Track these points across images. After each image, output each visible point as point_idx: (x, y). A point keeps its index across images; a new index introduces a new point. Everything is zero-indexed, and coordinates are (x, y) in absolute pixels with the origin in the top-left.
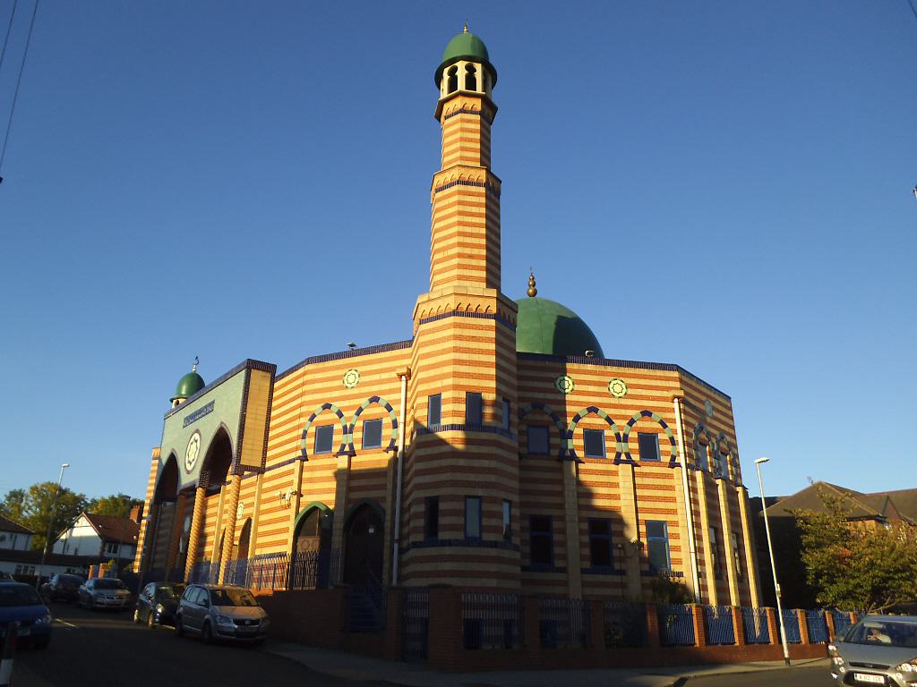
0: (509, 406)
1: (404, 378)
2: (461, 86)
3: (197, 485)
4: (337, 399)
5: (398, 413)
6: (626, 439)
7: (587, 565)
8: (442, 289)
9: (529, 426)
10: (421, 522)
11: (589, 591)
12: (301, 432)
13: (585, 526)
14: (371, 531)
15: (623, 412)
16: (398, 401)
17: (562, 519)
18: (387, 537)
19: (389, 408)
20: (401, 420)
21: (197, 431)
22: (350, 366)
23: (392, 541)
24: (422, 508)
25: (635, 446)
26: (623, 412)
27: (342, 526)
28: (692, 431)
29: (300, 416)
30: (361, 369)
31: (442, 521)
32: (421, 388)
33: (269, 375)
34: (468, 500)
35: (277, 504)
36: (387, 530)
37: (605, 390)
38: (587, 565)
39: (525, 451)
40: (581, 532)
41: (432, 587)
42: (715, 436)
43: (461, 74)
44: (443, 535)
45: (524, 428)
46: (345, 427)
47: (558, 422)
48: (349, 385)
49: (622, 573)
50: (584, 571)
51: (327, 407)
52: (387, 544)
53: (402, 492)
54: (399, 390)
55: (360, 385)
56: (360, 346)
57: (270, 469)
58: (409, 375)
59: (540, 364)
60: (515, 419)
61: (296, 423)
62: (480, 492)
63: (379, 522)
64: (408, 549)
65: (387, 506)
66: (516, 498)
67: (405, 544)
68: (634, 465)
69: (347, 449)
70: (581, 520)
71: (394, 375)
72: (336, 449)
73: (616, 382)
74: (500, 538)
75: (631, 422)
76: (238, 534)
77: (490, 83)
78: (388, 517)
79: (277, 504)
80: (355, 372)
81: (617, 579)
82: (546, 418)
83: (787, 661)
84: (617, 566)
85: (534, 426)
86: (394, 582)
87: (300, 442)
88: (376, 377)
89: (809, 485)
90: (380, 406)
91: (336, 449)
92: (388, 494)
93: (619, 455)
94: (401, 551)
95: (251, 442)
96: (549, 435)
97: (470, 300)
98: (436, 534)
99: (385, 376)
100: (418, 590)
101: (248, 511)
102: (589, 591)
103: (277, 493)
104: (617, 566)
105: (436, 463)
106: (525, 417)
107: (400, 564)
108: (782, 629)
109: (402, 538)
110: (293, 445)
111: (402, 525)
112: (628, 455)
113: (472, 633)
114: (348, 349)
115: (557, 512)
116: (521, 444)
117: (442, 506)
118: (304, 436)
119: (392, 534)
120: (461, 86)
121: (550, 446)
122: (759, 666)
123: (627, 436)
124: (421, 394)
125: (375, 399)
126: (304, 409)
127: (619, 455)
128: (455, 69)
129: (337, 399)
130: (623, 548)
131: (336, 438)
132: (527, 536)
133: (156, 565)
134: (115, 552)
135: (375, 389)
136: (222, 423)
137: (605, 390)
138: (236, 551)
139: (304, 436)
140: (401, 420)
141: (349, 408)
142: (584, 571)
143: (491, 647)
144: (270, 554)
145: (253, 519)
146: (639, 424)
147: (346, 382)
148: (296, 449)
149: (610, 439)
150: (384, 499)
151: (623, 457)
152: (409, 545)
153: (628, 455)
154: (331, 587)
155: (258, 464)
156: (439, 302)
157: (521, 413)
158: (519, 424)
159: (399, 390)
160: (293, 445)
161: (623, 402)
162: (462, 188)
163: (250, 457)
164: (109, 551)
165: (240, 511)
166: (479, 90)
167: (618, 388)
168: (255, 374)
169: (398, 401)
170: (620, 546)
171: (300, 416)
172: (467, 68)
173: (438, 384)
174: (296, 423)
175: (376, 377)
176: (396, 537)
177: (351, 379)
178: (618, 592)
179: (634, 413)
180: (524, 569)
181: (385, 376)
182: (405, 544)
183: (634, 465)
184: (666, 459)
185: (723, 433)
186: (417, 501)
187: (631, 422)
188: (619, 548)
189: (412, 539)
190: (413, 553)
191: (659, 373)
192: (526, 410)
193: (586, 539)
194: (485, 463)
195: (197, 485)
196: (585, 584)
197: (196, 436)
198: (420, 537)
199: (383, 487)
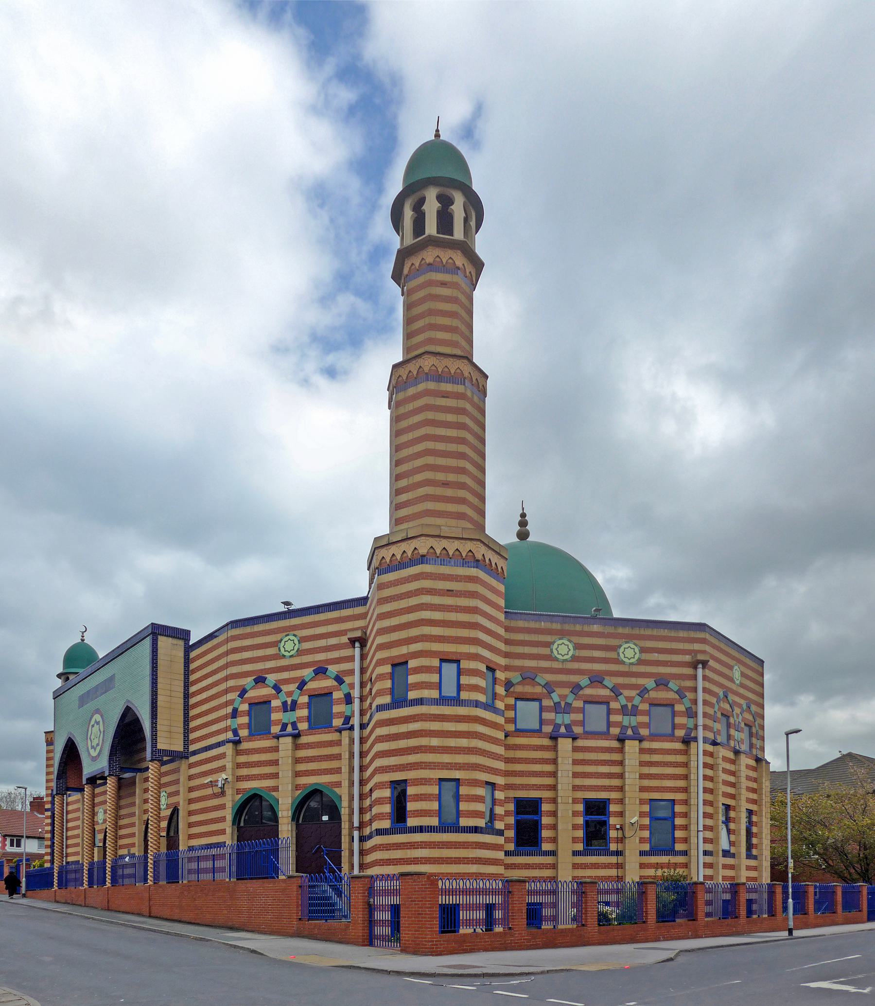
0: (493, 675)
1: (357, 644)
2: (431, 228)
3: (107, 774)
5: (352, 686)
6: (294, 706)
7: (580, 847)
8: (407, 529)
9: (517, 699)
10: (387, 808)
11: (580, 873)
12: (229, 709)
13: (580, 807)
14: (325, 818)
15: (633, 681)
16: (351, 672)
18: (345, 826)
19: (339, 680)
20: (356, 693)
21: (97, 711)
22: (286, 630)
23: (351, 828)
24: (387, 793)
26: (633, 681)
27: (290, 814)
28: (714, 700)
29: (227, 691)
30: (576, 640)
31: (411, 806)
32: (380, 655)
33: (181, 643)
34: (443, 783)
35: (209, 791)
36: (345, 817)
37: (545, 651)
38: (580, 847)
39: (511, 727)
40: (575, 814)
41: (403, 875)
42: (740, 706)
43: (431, 207)
44: (411, 822)
45: (511, 701)
46: (285, 703)
47: (621, 698)
48: (286, 654)
51: (260, 680)
52: (345, 832)
53: (361, 776)
54: (351, 659)
55: (300, 653)
56: (296, 606)
57: (195, 753)
58: (362, 641)
60: (500, 690)
61: (223, 699)
62: (457, 775)
63: (334, 811)
64: (370, 837)
65: (343, 792)
66: (500, 780)
67: (367, 831)
69: (289, 729)
70: (575, 801)
71: (344, 639)
73: (626, 645)
74: (481, 823)
75: (302, 684)
76: (164, 824)
77: (473, 223)
78: (345, 803)
79: (209, 791)
80: (292, 638)
81: (613, 859)
82: (538, 690)
83: (790, 932)
85: (522, 699)
86: (356, 872)
87: (229, 722)
88: (322, 643)
89: (839, 755)
90: (329, 677)
92: (344, 777)
94: (362, 839)
95: (167, 723)
96: (674, 714)
97: (445, 543)
98: (405, 821)
99: (333, 641)
100: (383, 877)
101: (174, 800)
102: (580, 873)
103: (207, 780)
104: (613, 847)
105: (402, 744)
106: (512, 689)
107: (362, 853)
108: (790, 900)
109: (362, 826)
110: (222, 725)
111: (362, 811)
113: (449, 918)
114: (282, 608)
115: (613, 795)
116: (508, 721)
117: (411, 791)
118: (235, 714)
119: (351, 822)
120: (431, 228)
121: (674, 727)
122: (762, 937)
123: (296, 701)
124: (381, 662)
126: (231, 683)
128: (422, 201)
130: (621, 828)
132: (511, 820)
133: (70, 859)
134: (18, 845)
136: (128, 701)
137: (545, 651)
138: (164, 842)
140: (356, 693)
141: (562, 684)
142: (575, 853)
143: (471, 931)
144: (207, 845)
145: (181, 808)
147: (282, 650)
148: (226, 730)
149: (277, 710)
150: (338, 784)
152: (371, 833)
153: (568, 727)
154: (281, 877)
155: (180, 748)
156: (404, 546)
157: (508, 685)
158: (506, 696)
159: (351, 659)
160: (222, 725)
161: (635, 669)
162: (432, 385)
163: (169, 739)
164: (12, 845)
165: (163, 801)
166: (458, 234)
168: (164, 642)
169: (351, 672)
170: (618, 827)
171: (227, 691)
172: (439, 198)
173: (404, 650)
174: (223, 699)
175: (322, 643)
176: (356, 824)
177: (289, 646)
178: (613, 872)
180: (507, 853)
181: (333, 641)
182: (367, 831)
184: (337, 722)
185: (750, 702)
186: (380, 786)
187: (302, 684)
188: (617, 829)
189: (376, 825)
190: (377, 840)
191: (682, 634)
192: (514, 681)
193: (580, 821)
194: (464, 742)
195: (107, 774)
196: (642, 866)
197: (97, 717)
198: (386, 824)
199: (338, 771)
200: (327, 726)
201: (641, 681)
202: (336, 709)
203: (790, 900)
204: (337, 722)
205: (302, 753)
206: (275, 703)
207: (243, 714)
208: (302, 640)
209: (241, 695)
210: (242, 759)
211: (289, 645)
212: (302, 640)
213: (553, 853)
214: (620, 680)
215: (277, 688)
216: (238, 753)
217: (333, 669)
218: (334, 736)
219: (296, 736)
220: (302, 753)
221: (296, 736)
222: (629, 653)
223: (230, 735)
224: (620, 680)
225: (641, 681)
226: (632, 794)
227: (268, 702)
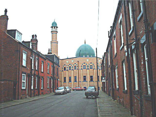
4: (93, 62)
7: (90, 81)
13: (90, 77)
17: (87, 76)
30: (89, 59)
49: (72, 82)
50: (63, 82)
55: (89, 61)
59: (75, 58)
68: (89, 69)
72: (66, 70)
81: (93, 82)
84: (93, 81)
91: (66, 70)
93: (87, 68)
98: (64, 79)
112: (88, 68)
125: (70, 64)
127: (87, 68)
129: (93, 62)
131: (66, 69)
135: (70, 63)
139: (62, 68)
142: (63, 82)
146: (83, 64)
151: (88, 69)
153: (88, 68)
167: (88, 60)
183: (89, 69)
184: (86, 69)
187: (89, 64)
200: (92, 69)
201: (89, 63)
202: (77, 67)
203: (149, 86)
204: (93, 68)
205: (74, 72)
206: (71, 67)
208: (68, 61)
210: (68, 72)
211: (72, 61)
212: (68, 61)
213: (87, 81)
214: (87, 63)
215: (71, 65)
216: (68, 72)
217: (92, 63)
218: (76, 70)
219: (73, 70)
220: (74, 72)
221: (73, 70)
223: (62, 70)
224: (87, 63)
225: (89, 63)
226: (88, 75)
227: (85, 66)
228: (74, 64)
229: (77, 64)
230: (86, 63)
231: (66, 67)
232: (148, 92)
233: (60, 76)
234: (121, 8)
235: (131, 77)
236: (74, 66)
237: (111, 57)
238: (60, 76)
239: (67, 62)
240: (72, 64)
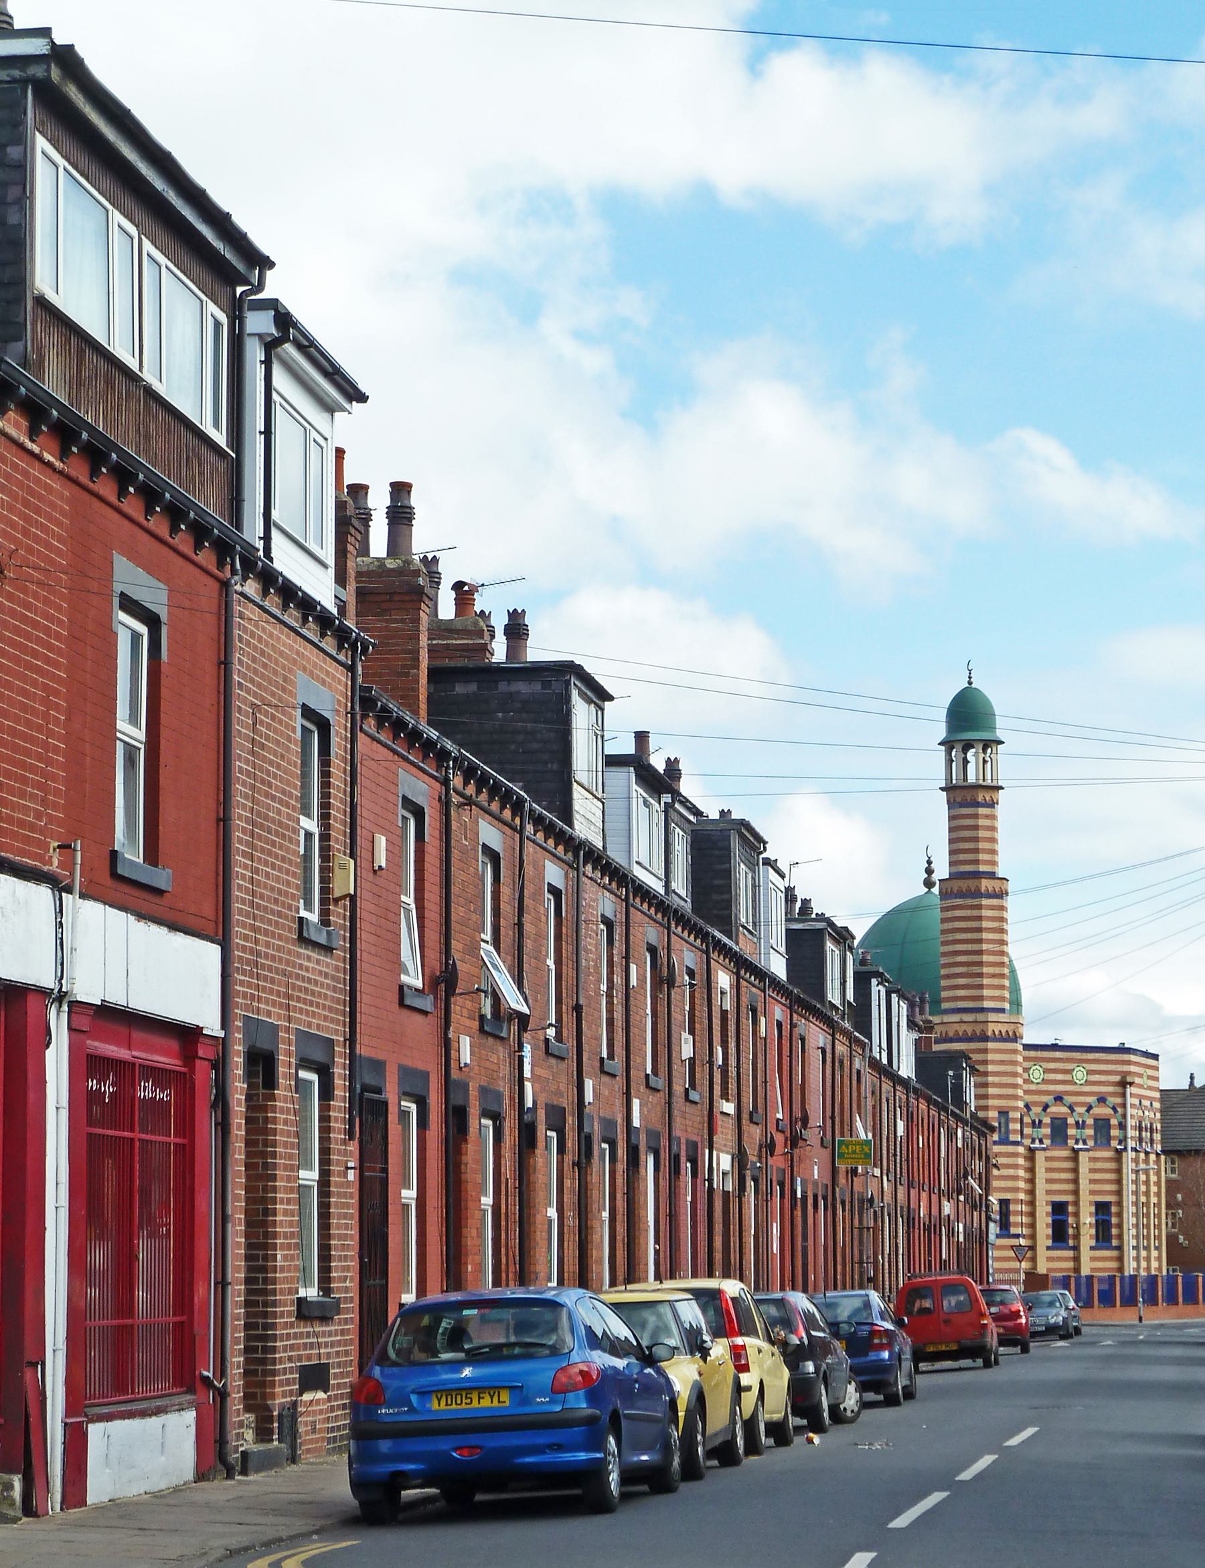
25: (1048, 1131)
26: (1036, 1098)
30: (1045, 1065)
37: (1068, 1077)
55: (1087, 1083)
56: (163, 931)
117: (1012, 1207)
137: (1068, 1077)
146: (1052, 1109)
179: (1048, 1099)
187: (1090, 1108)
207: (1089, 1127)
208: (1089, 1072)
209: (1088, 1111)
211: (1080, 1074)
222: (1080, 1075)
228: (1091, 1100)
229: (1114, 1109)
230: (1069, 1099)
231: (1070, 1121)
232: (576, 1496)
233: (242, 983)
234: (395, 752)
235: (727, 1076)
236: (1096, 1120)
237: (316, 348)
238: (242, 983)
239: (1080, 1074)
240: (1036, 1098)
